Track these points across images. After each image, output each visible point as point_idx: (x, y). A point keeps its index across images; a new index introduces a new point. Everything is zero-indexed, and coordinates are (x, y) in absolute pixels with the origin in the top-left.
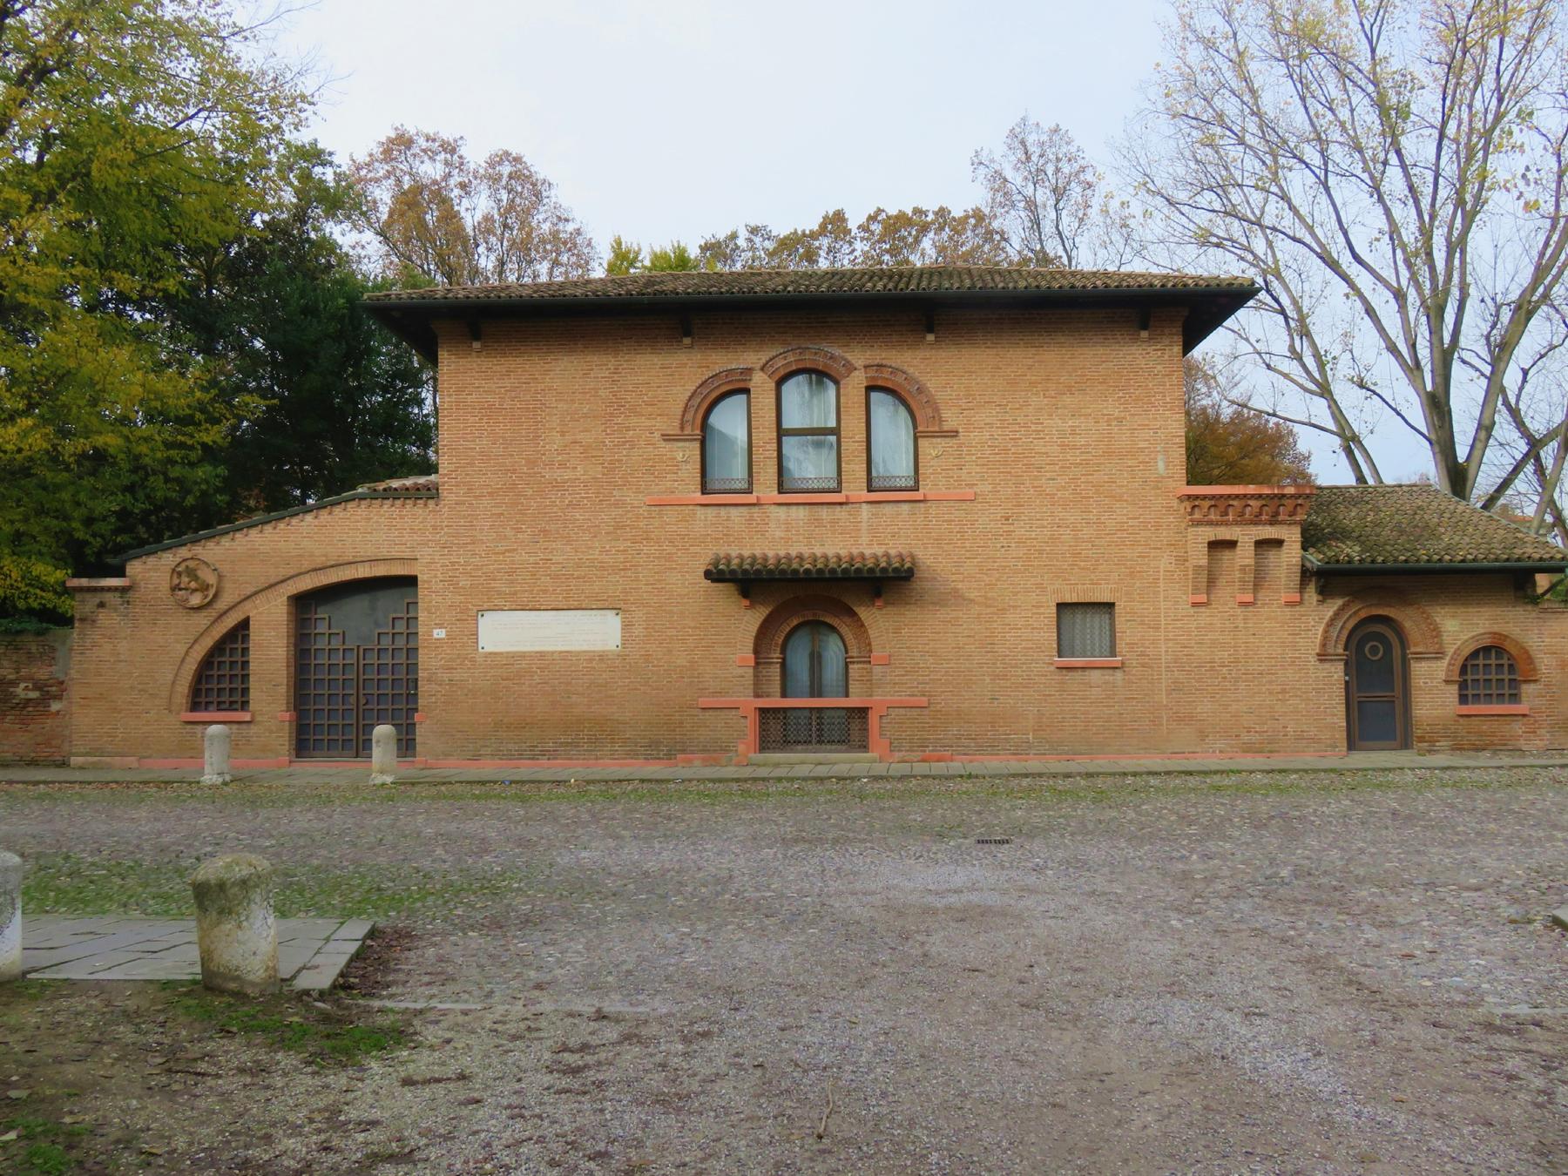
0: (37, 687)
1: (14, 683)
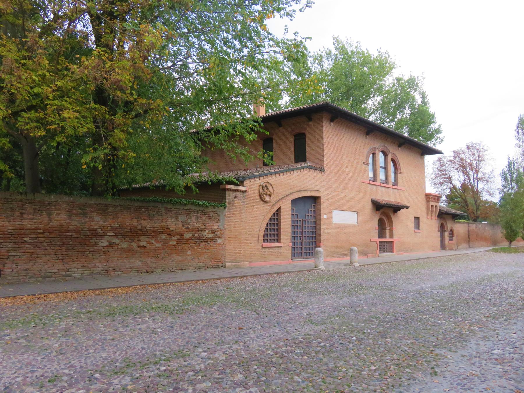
0: (213, 233)
1: (204, 230)
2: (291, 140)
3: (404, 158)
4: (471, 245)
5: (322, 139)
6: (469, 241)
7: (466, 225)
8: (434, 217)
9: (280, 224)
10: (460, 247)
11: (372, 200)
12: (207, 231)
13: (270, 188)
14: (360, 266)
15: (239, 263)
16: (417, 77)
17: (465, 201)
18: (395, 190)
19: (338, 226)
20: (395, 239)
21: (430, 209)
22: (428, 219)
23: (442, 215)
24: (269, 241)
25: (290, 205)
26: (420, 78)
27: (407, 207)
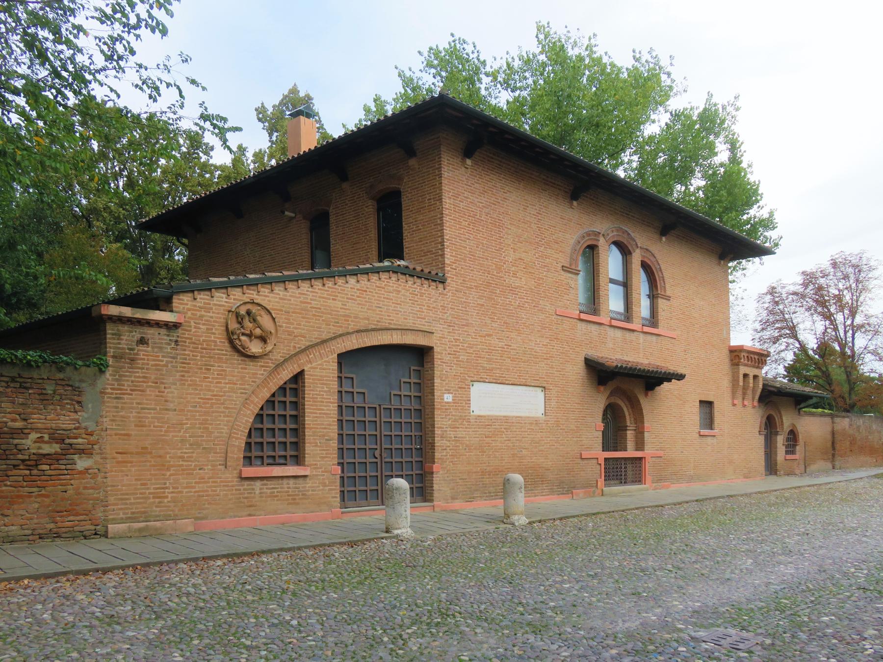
1: (21, 433)
2: (369, 209)
3: (677, 263)
4: (837, 463)
5: (440, 200)
6: (833, 455)
7: (828, 420)
8: (751, 402)
9: (304, 417)
10: (813, 468)
11: (585, 358)
12: (34, 436)
13: (265, 321)
14: (530, 523)
15: (158, 524)
16: (724, 108)
17: (826, 375)
18: (649, 337)
19: (487, 422)
20: (649, 451)
21: (741, 384)
22: (734, 405)
23: (771, 397)
24: (266, 461)
25: (335, 366)
26: (729, 109)
27: (680, 377)
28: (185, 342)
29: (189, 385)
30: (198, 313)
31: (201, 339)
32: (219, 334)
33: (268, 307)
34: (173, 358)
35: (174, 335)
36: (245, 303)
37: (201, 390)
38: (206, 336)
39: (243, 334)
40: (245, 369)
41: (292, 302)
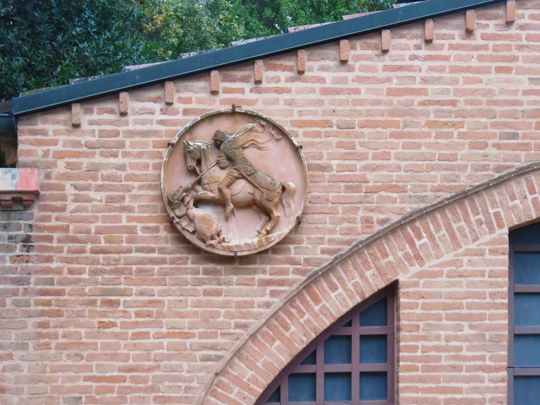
13: (272, 161)
25: (502, 262)
28: (50, 239)
29: (61, 347)
30: (85, 161)
31: (93, 227)
32: (142, 208)
33: (276, 119)
34: (18, 282)
35: (21, 225)
36: (211, 117)
37: (91, 358)
38: (105, 219)
39: (199, 202)
40: (218, 293)
41: (364, 96)
